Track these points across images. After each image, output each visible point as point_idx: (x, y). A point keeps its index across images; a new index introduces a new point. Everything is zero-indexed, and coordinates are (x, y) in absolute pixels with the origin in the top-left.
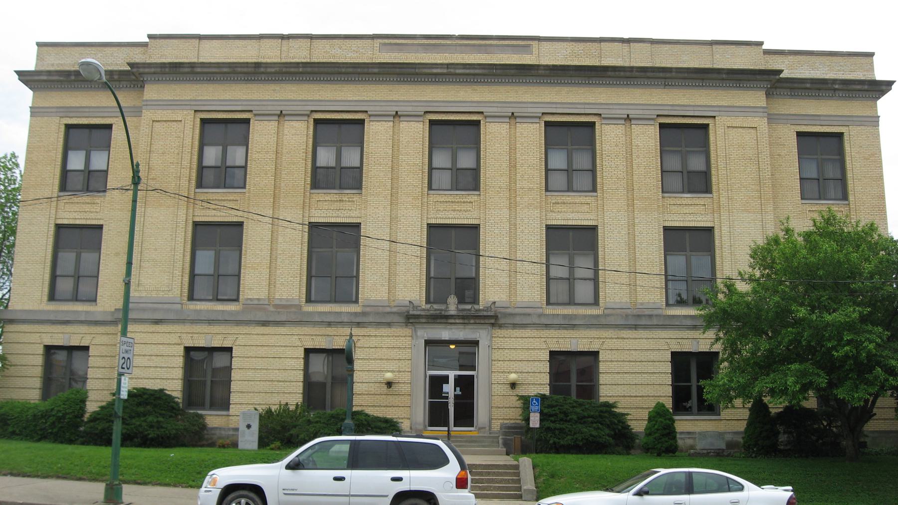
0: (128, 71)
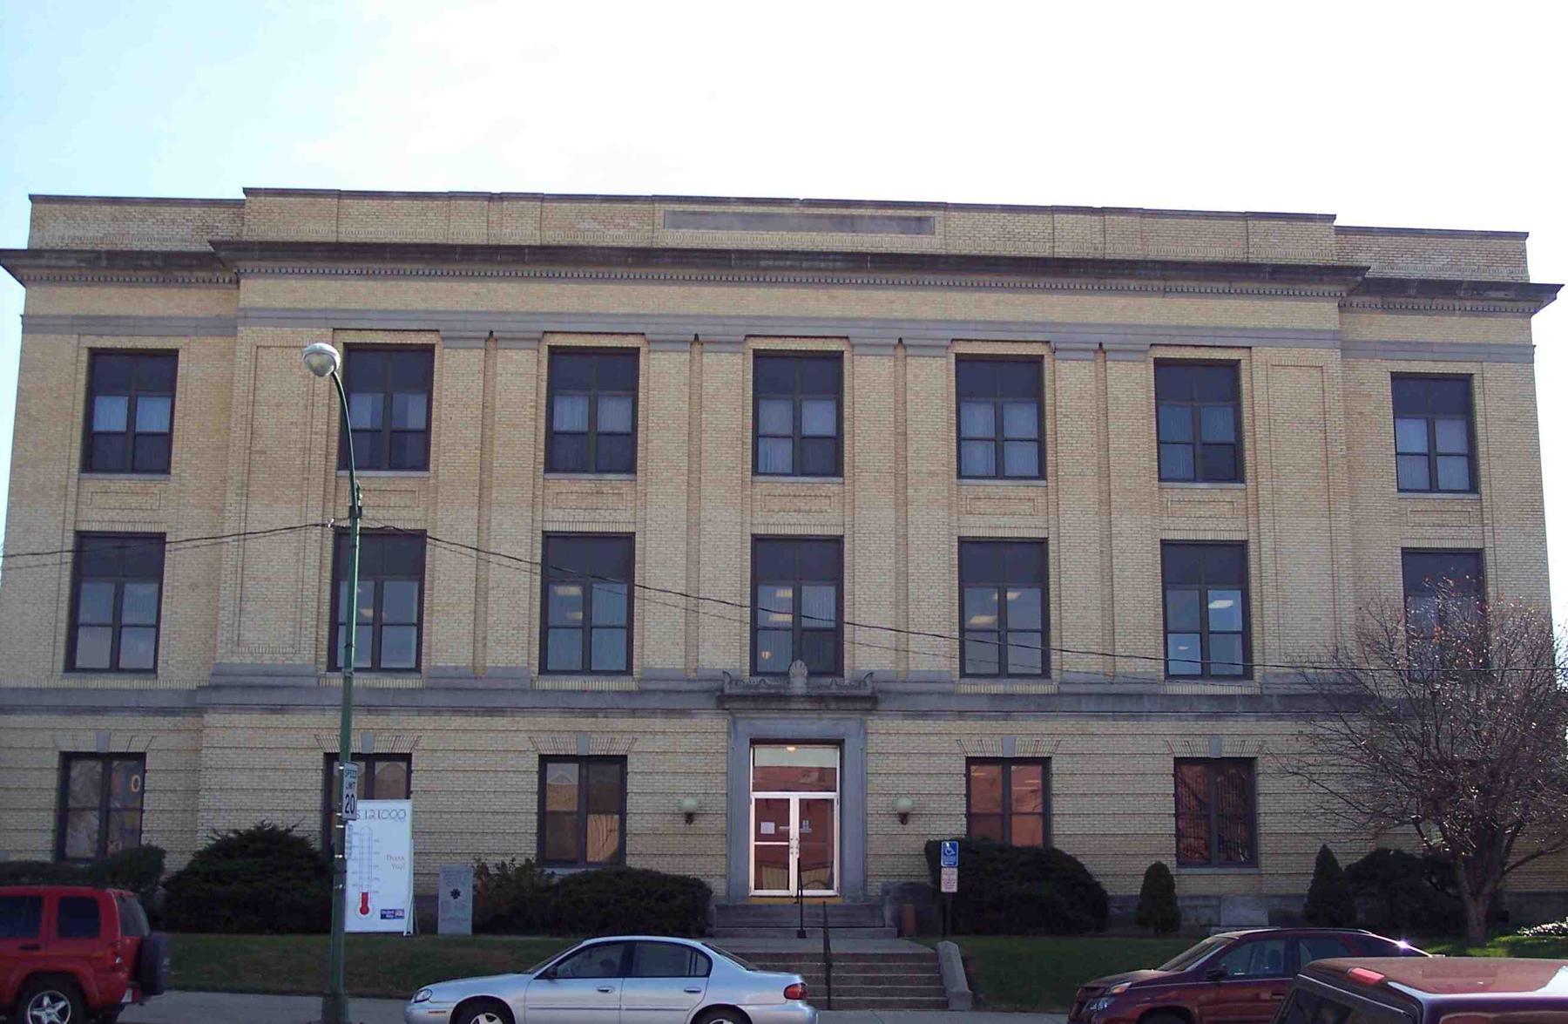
0: (205, 254)
